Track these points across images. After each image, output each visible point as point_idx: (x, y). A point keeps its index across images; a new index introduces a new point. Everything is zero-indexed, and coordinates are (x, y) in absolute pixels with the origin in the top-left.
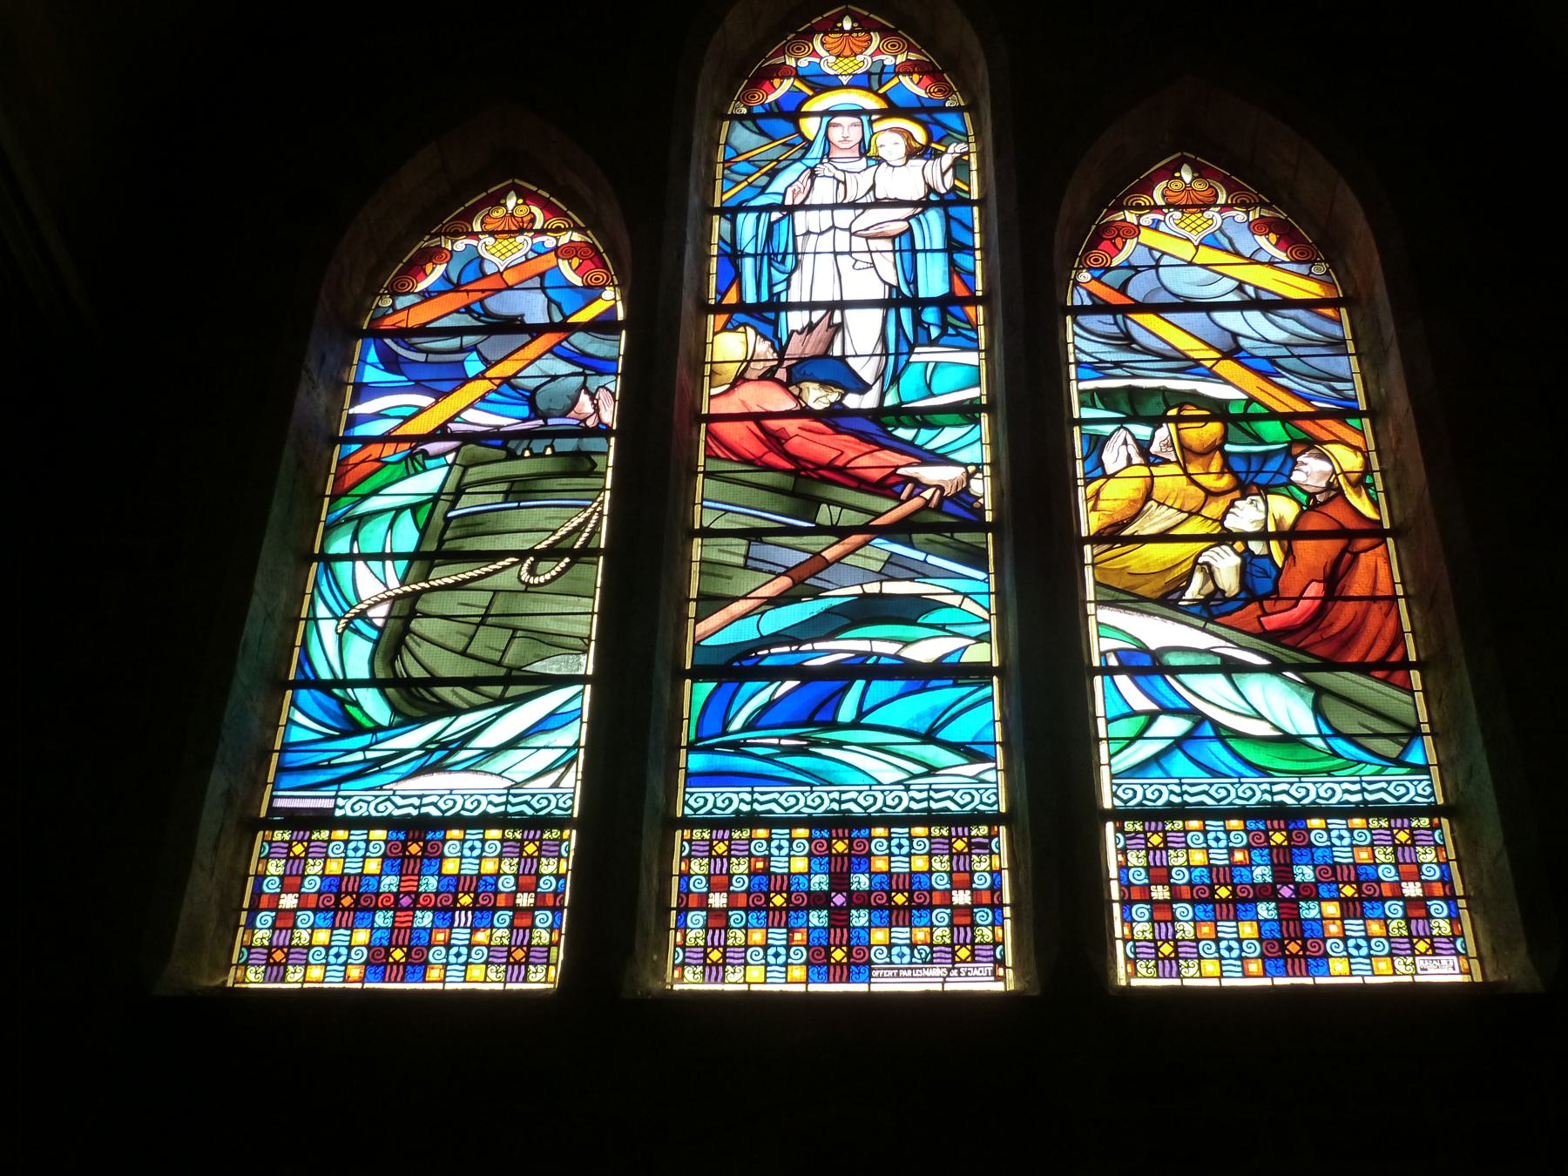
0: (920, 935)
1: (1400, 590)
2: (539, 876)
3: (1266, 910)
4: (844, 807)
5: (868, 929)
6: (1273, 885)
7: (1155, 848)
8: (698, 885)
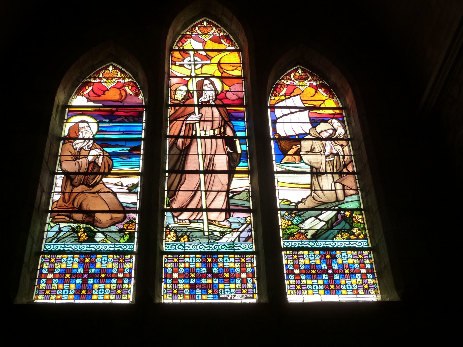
0: (108, 286)
1: (359, 189)
2: (179, 268)
3: (325, 277)
4: (90, 249)
5: (218, 284)
6: (327, 270)
7: (295, 259)
8: (170, 271)
